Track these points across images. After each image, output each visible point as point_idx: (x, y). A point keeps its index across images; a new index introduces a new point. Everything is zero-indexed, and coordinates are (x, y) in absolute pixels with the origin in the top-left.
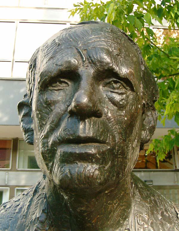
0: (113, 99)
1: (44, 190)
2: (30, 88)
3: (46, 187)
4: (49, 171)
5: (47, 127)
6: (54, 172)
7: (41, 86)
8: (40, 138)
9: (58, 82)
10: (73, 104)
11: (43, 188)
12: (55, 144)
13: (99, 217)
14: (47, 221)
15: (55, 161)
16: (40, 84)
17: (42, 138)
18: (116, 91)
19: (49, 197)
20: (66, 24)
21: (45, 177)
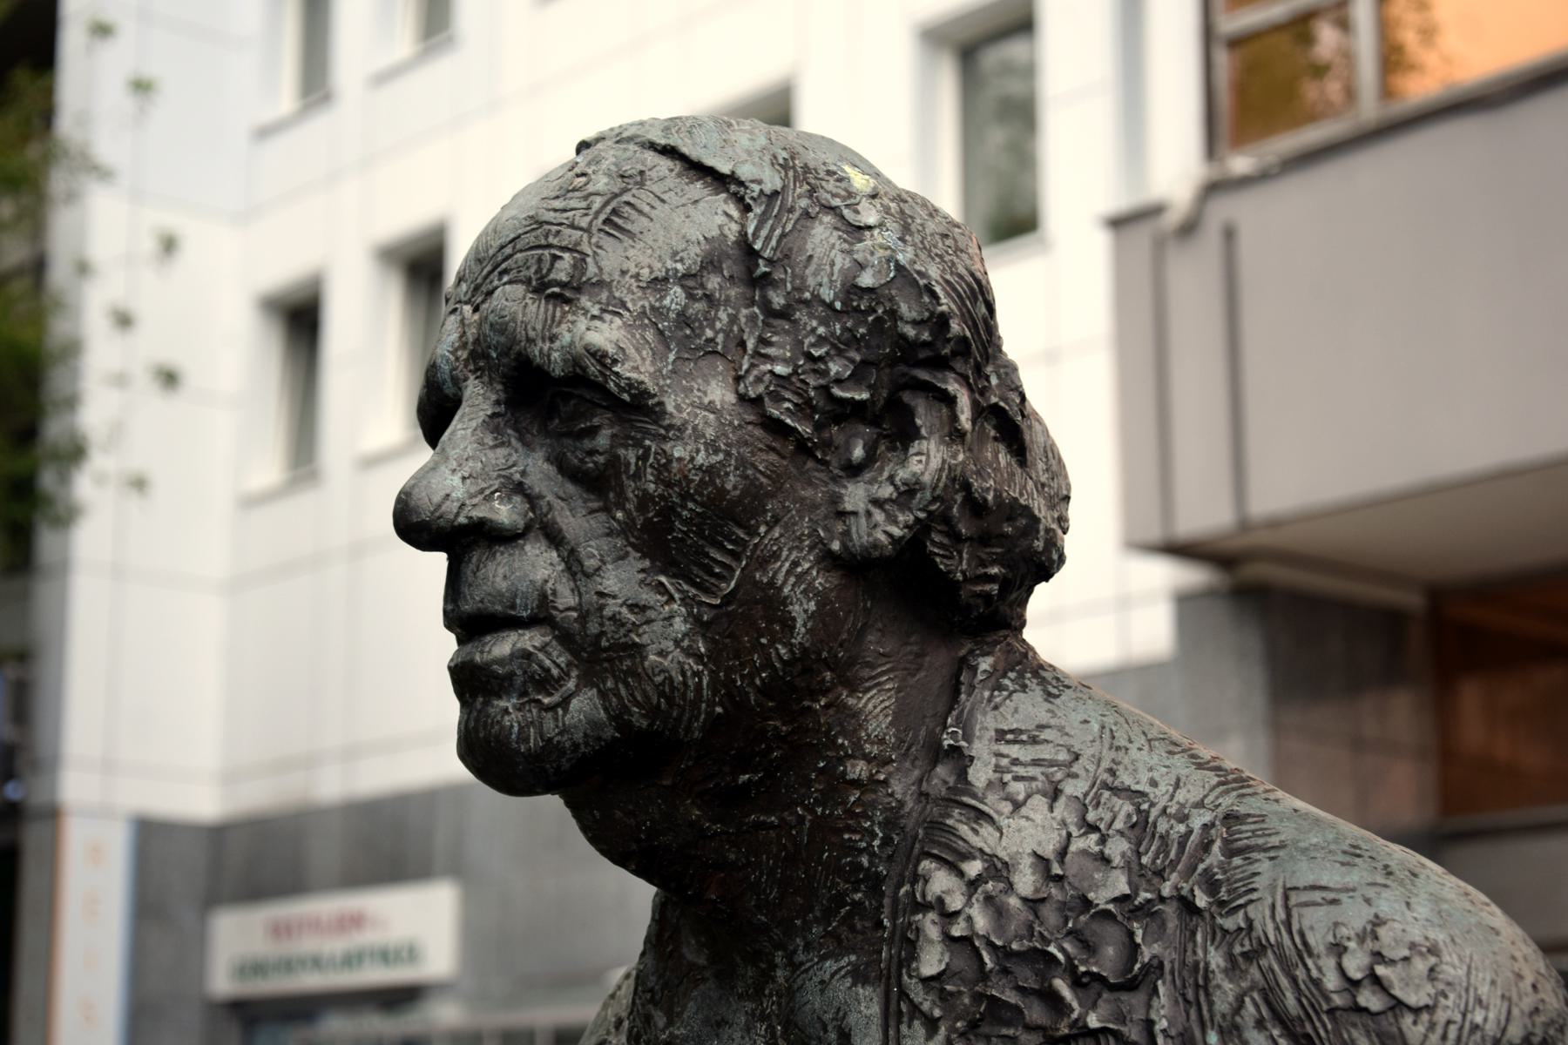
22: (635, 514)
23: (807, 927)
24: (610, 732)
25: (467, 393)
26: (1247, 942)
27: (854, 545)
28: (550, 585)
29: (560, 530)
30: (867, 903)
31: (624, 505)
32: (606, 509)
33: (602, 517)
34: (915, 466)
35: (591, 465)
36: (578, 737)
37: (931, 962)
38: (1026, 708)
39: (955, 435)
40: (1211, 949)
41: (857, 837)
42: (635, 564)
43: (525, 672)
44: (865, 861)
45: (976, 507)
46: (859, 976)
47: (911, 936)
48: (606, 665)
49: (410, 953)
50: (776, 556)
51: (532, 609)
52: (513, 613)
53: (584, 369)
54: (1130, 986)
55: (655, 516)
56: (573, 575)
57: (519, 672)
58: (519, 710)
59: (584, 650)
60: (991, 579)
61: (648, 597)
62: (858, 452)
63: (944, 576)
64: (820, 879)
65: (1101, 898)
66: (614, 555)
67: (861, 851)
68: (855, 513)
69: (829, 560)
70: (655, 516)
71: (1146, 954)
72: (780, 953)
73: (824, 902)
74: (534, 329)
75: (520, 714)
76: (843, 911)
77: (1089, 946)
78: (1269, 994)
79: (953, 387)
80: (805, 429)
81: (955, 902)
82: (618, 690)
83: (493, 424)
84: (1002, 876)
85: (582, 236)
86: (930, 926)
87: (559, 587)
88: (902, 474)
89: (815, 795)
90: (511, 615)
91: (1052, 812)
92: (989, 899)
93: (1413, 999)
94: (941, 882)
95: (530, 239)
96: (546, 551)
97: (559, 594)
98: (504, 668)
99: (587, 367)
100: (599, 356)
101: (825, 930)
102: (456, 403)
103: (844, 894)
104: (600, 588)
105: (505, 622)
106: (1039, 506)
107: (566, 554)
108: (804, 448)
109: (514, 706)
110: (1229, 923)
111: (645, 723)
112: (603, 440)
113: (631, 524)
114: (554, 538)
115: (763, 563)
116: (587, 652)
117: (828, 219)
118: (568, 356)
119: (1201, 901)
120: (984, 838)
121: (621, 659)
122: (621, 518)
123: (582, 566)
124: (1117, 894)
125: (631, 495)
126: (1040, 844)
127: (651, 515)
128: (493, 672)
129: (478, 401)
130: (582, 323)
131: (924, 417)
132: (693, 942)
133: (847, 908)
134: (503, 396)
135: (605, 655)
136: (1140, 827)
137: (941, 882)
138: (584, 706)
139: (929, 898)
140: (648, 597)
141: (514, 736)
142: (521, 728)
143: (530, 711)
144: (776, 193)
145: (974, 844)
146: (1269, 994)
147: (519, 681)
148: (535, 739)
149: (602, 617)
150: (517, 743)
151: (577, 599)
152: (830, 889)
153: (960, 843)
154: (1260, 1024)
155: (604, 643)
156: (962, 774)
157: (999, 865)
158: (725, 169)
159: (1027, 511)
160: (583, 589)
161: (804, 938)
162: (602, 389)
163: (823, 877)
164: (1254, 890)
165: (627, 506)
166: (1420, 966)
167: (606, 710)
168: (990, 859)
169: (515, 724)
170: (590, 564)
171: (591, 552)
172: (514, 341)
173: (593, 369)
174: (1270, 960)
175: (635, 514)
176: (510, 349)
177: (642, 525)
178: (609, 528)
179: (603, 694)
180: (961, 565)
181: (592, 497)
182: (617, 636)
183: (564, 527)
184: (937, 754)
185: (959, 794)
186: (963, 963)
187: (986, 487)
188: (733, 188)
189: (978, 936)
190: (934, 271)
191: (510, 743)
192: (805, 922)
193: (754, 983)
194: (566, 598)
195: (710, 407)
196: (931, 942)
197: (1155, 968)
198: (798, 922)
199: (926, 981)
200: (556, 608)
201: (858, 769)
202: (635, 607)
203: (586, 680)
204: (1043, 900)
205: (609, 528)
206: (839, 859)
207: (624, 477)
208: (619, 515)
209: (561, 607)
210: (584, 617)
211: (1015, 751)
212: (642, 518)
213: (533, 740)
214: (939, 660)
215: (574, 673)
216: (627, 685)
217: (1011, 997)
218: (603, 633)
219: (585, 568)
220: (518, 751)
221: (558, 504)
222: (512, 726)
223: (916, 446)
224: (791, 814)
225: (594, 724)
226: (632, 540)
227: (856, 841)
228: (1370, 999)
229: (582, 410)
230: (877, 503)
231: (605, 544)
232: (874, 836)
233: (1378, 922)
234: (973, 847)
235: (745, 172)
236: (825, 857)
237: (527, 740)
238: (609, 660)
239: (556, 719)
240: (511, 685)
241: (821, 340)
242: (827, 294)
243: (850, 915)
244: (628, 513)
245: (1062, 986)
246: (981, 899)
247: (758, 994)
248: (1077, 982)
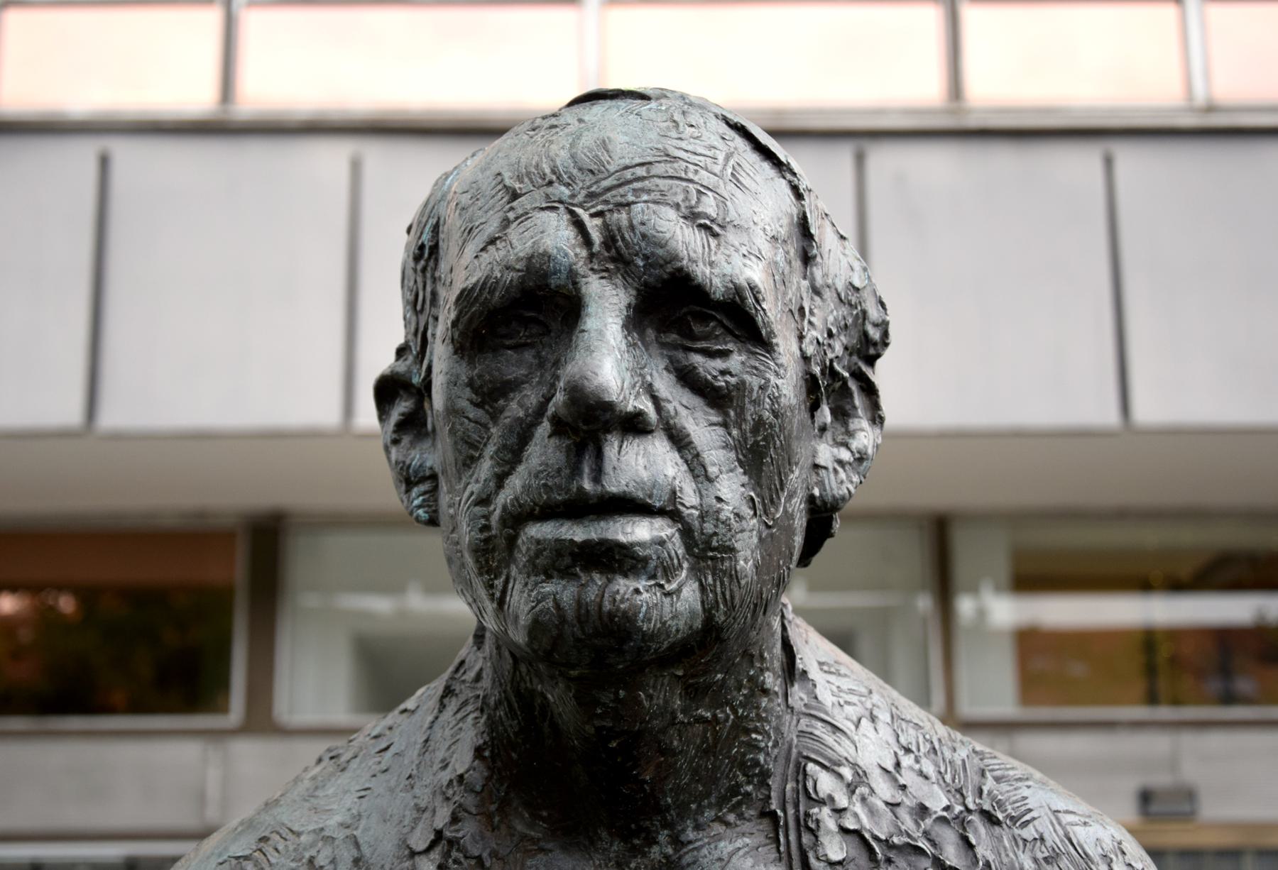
0: (690, 371)
1: (479, 685)
2: (421, 329)
3: (484, 675)
4: (495, 605)
5: (485, 468)
6: (511, 604)
7: (462, 334)
8: (462, 503)
9: (514, 323)
10: (560, 397)
11: (478, 678)
12: (518, 518)
13: (661, 762)
14: (490, 783)
15: (514, 571)
16: (461, 326)
17: (469, 502)
18: (704, 345)
19: (498, 703)
20: (458, 740)
21: (482, 643)
22: (748, 435)
23: (700, 810)
26: (1043, 849)
27: (827, 495)
28: (677, 482)
29: (688, 435)
30: (754, 795)
31: (741, 425)
32: (725, 425)
33: (721, 431)
35: (723, 384)
36: (681, 624)
40: (1020, 853)
41: (760, 738)
42: (739, 477)
43: (658, 558)
44: (761, 758)
47: (813, 826)
48: (710, 562)
51: (664, 501)
52: (650, 502)
53: (743, 299)
55: (762, 440)
56: (695, 477)
57: (654, 557)
58: (647, 591)
59: (697, 545)
64: (724, 771)
66: (727, 468)
67: (760, 750)
68: (825, 468)
70: (762, 440)
72: (666, 832)
73: (722, 791)
74: (695, 252)
75: (648, 595)
76: (735, 800)
77: (935, 844)
81: (842, 801)
82: (715, 587)
84: (864, 782)
85: (718, 181)
87: (683, 484)
89: (741, 698)
90: (647, 503)
91: (878, 733)
92: (863, 799)
96: (859, 465)
97: (684, 492)
98: (645, 551)
99: (747, 298)
100: (754, 289)
101: (716, 815)
103: (738, 786)
104: (719, 494)
107: (690, 457)
109: (644, 587)
111: (723, 618)
113: (743, 443)
114: (679, 441)
116: (699, 549)
118: (731, 285)
121: (723, 559)
122: (736, 437)
123: (706, 471)
124: (944, 805)
125: (749, 418)
126: (880, 758)
127: (760, 438)
128: (635, 552)
132: (527, 815)
133: (740, 797)
134: (634, 302)
135: (711, 554)
139: (821, 795)
141: (641, 615)
142: (648, 608)
143: (655, 594)
145: (841, 754)
147: (652, 564)
148: (656, 621)
149: (718, 519)
150: (643, 621)
151: (698, 499)
152: (731, 780)
153: (830, 751)
155: (714, 544)
157: (861, 773)
160: (704, 492)
161: (696, 820)
163: (727, 770)
164: (1030, 810)
165: (744, 427)
167: (703, 602)
169: (644, 604)
170: (713, 470)
175: (748, 435)
176: (670, 262)
177: (752, 445)
178: (724, 442)
179: (703, 588)
181: (712, 411)
182: (725, 539)
183: (692, 433)
188: (789, 176)
189: (865, 829)
191: (636, 621)
192: (699, 806)
193: (617, 857)
194: (689, 496)
196: (829, 832)
198: (693, 806)
200: (683, 505)
203: (696, 572)
204: (898, 805)
205: (724, 442)
206: (744, 755)
207: (747, 400)
208: (735, 432)
209: (688, 504)
210: (702, 517)
212: (753, 439)
215: (685, 565)
216: (722, 583)
218: (715, 534)
219: (709, 474)
220: (640, 629)
221: (683, 412)
222: (642, 606)
224: (722, 712)
226: (741, 457)
227: (759, 741)
229: (717, 333)
230: (841, 463)
232: (769, 737)
234: (840, 756)
236: (733, 752)
237: (650, 620)
238: (712, 558)
239: (672, 605)
240: (644, 568)
243: (739, 804)
244: (743, 433)
246: (859, 799)
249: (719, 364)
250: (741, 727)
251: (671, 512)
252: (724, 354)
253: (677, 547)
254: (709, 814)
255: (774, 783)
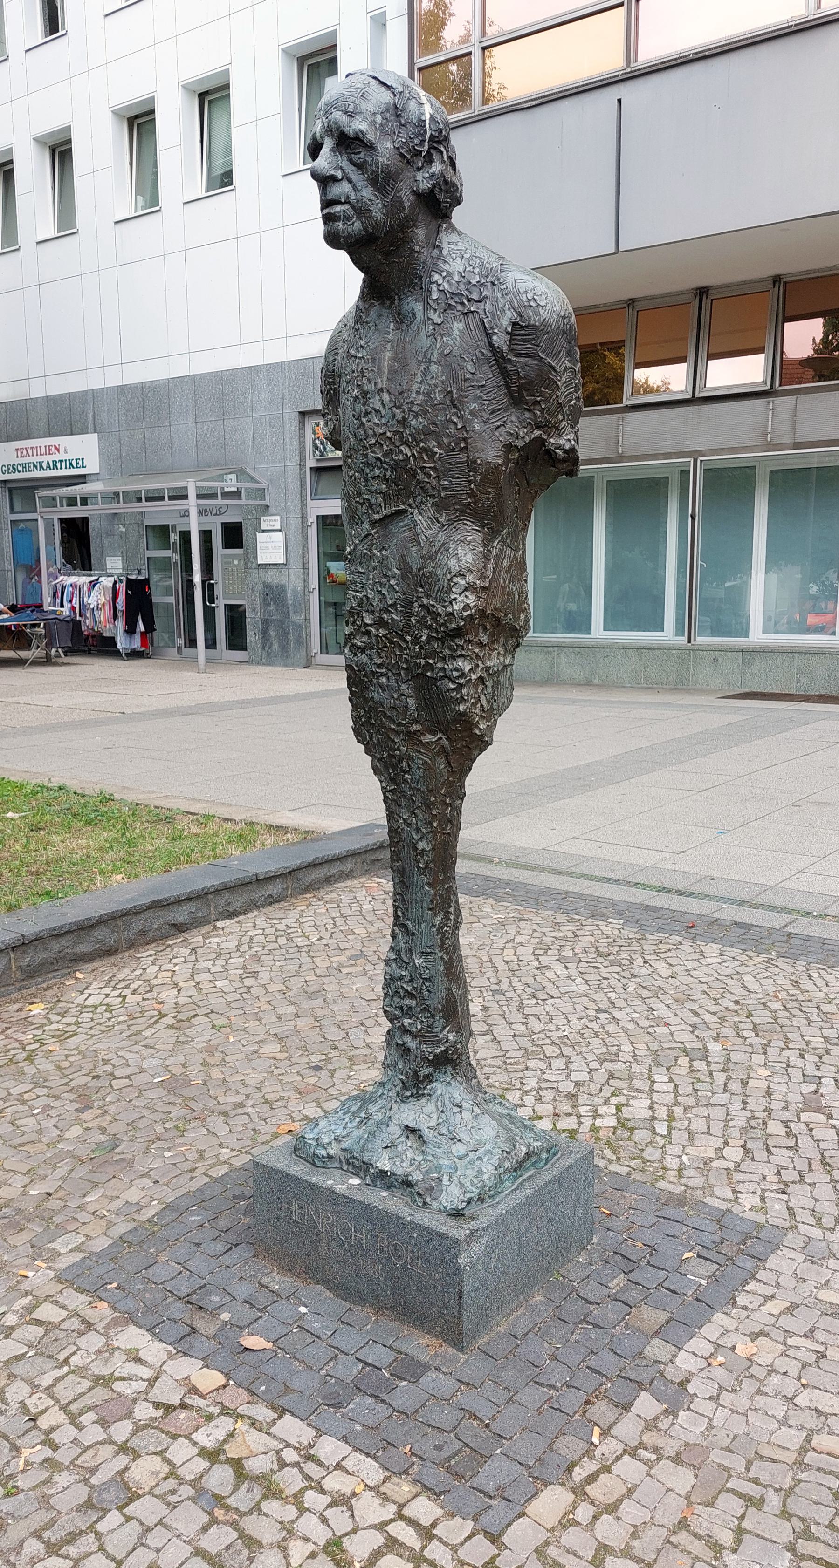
23: (404, 289)
24: (363, 233)
25: (325, 141)
34: (433, 169)
37: (435, 296)
38: (454, 238)
39: (443, 162)
42: (370, 189)
45: (446, 182)
46: (416, 300)
49: (80, 463)
50: (401, 190)
54: (480, 301)
60: (447, 202)
61: (373, 198)
62: (420, 165)
63: (438, 200)
65: (474, 282)
69: (415, 193)
71: (483, 294)
78: (511, 302)
79: (442, 149)
80: (409, 157)
81: (440, 282)
83: (332, 150)
86: (434, 287)
88: (431, 171)
92: (448, 281)
93: (541, 304)
94: (436, 277)
95: (341, 99)
100: (362, 132)
102: (322, 145)
105: (337, 202)
106: (458, 184)
108: (408, 162)
110: (502, 287)
112: (362, 155)
114: (350, 181)
115: (399, 191)
117: (414, 100)
119: (496, 282)
120: (446, 267)
129: (328, 145)
130: (358, 123)
131: (436, 156)
136: (482, 264)
137: (436, 277)
138: (357, 225)
140: (373, 198)
144: (401, 92)
146: (511, 302)
154: (509, 309)
156: (441, 252)
158: (389, 84)
159: (456, 185)
162: (362, 141)
166: (544, 297)
168: (448, 272)
170: (359, 188)
171: (359, 185)
172: (340, 127)
173: (361, 136)
174: (511, 295)
180: (441, 197)
184: (435, 247)
185: (440, 257)
186: (443, 296)
187: (448, 176)
190: (439, 117)
194: (353, 196)
195: (387, 148)
197: (486, 297)
199: (434, 300)
201: (417, 248)
202: (370, 200)
203: (359, 218)
210: (358, 202)
211: (452, 247)
213: (346, 234)
214: (434, 223)
217: (454, 304)
223: (434, 164)
225: (359, 230)
228: (533, 304)
231: (363, 183)
233: (535, 287)
235: (394, 86)
241: (413, 133)
242: (414, 121)
245: (465, 301)
247: (390, 307)
248: (469, 301)
249: (358, 156)
250: (409, 263)
251: (347, 202)
252: (359, 153)
253: (351, 212)
254: (406, 290)
255: (423, 279)
